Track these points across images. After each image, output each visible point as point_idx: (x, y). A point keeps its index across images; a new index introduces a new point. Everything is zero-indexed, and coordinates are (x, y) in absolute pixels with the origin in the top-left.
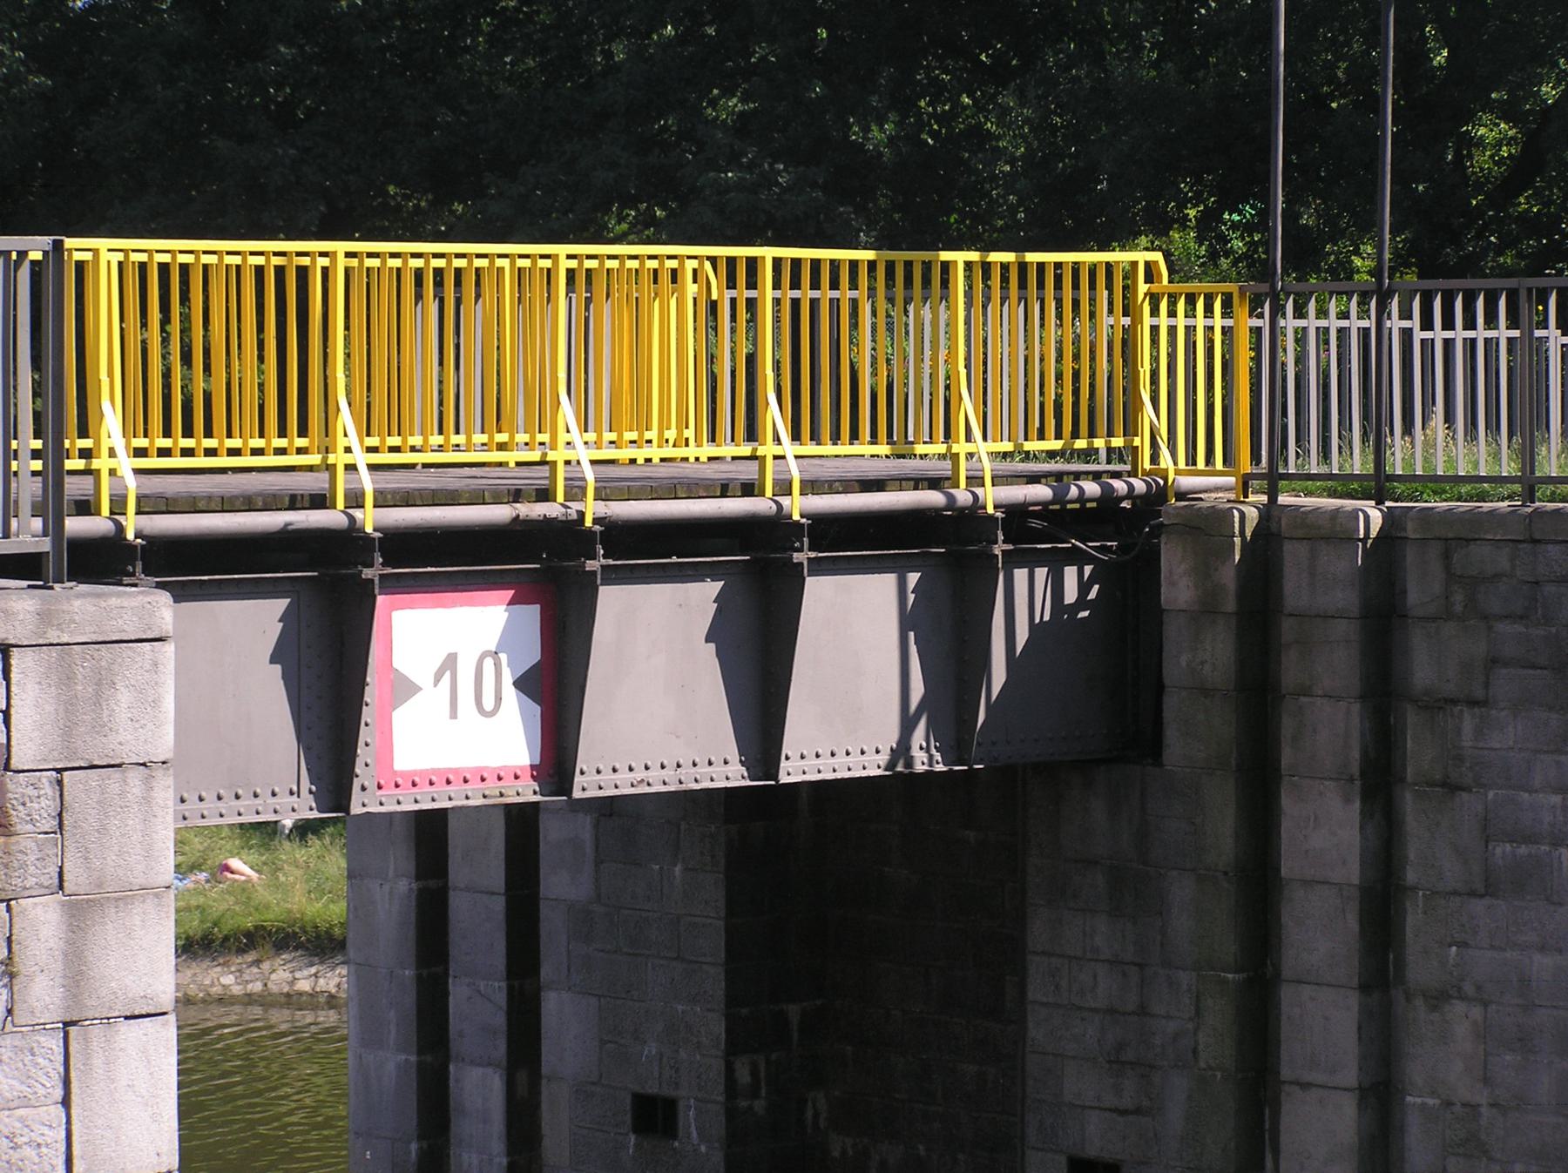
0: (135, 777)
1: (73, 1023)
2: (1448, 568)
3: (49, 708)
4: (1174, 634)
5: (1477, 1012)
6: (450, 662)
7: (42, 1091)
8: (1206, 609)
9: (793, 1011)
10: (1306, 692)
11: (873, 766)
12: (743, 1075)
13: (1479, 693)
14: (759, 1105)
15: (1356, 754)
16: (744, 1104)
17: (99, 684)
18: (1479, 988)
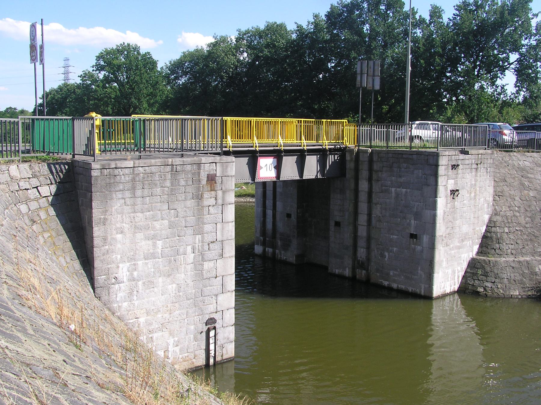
4: (348, 163)
5: (380, 206)
8: (351, 160)
12: (299, 211)
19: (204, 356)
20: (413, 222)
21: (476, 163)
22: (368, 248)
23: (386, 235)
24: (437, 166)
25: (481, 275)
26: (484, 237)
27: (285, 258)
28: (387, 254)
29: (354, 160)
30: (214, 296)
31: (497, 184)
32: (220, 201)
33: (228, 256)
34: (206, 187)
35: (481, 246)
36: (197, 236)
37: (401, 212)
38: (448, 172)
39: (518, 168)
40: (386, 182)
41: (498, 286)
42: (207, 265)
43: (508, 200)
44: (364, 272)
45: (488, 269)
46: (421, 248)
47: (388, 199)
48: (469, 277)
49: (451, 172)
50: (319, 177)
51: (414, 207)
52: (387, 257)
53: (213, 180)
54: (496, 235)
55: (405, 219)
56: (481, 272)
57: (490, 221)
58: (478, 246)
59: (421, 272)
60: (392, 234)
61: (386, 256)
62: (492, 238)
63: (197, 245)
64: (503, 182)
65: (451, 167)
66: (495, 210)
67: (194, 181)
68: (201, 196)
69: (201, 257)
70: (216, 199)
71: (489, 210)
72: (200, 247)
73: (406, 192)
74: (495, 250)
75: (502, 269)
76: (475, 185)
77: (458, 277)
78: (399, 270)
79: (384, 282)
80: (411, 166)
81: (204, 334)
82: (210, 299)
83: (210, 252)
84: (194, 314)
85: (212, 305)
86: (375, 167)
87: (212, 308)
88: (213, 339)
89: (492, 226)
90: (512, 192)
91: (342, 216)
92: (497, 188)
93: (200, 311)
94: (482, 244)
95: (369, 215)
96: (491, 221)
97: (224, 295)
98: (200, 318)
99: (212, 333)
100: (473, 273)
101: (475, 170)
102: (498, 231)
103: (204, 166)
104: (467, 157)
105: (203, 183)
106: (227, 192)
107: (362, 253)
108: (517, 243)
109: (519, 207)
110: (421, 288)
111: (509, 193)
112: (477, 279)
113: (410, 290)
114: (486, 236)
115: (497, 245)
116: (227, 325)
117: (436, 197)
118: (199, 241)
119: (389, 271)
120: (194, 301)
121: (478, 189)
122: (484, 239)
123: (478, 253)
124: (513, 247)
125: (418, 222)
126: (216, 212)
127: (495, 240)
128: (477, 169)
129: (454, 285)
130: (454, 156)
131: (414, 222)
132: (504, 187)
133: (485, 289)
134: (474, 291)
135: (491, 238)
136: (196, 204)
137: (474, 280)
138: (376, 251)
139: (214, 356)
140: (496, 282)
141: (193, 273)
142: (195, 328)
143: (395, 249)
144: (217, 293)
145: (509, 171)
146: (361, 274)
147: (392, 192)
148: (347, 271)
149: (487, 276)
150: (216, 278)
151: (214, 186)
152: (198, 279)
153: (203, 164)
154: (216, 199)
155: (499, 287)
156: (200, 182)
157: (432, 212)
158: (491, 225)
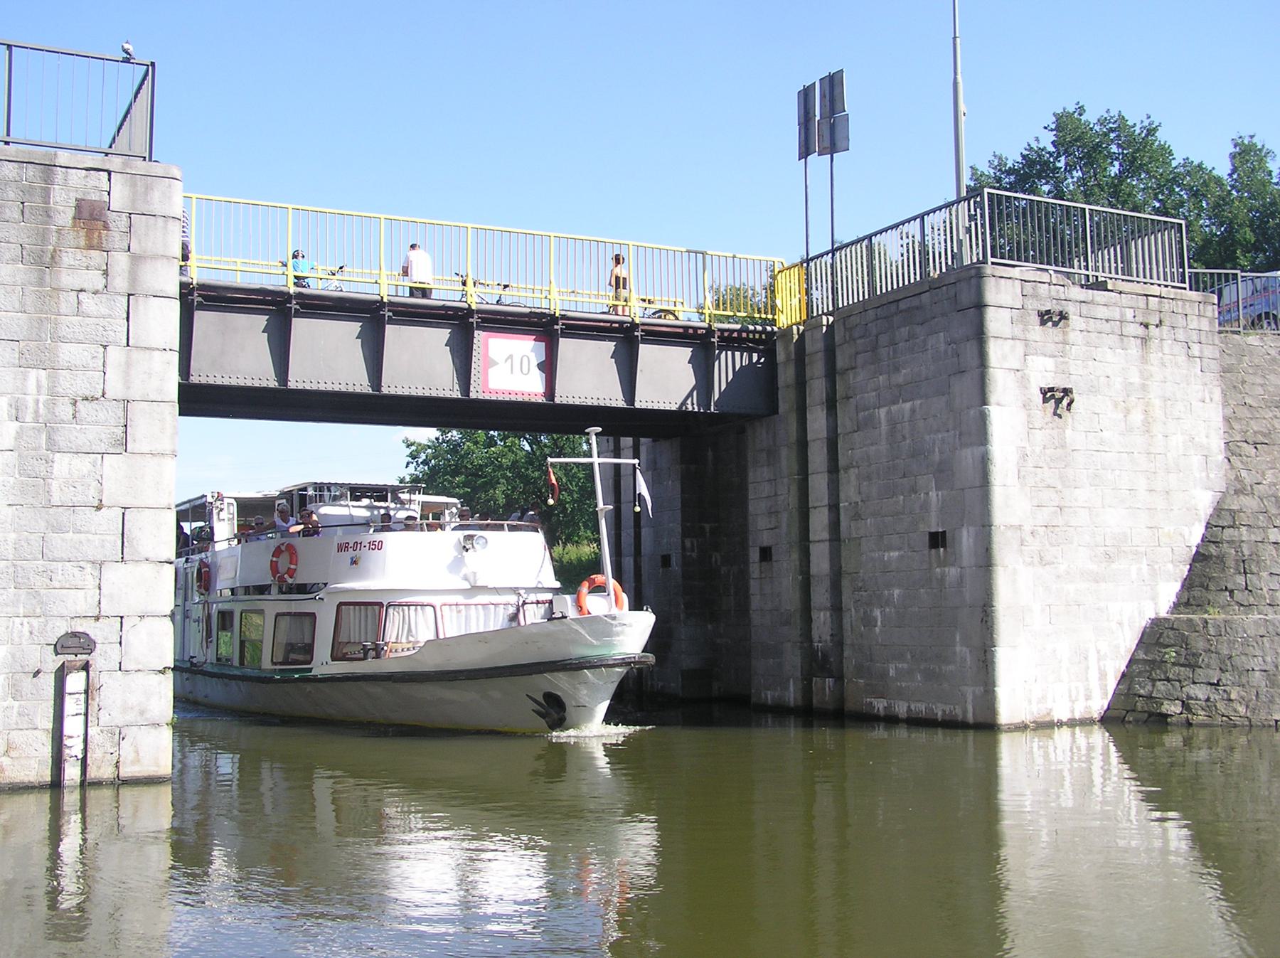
0: (160, 220)
1: (133, 295)
5: (856, 470)
6: (511, 357)
7: (117, 314)
8: (788, 360)
9: (707, 526)
11: (674, 407)
12: (688, 544)
13: (854, 365)
14: (694, 555)
15: (824, 395)
16: (689, 554)
17: (147, 188)
18: (857, 462)
19: (47, 751)
20: (935, 495)
21: (1139, 319)
22: (837, 609)
23: (873, 555)
25: (1174, 664)
27: (661, 684)
28: (877, 613)
30: (89, 565)
31: (1252, 414)
32: (120, 282)
34: (70, 237)
35: (1188, 584)
36: (33, 373)
37: (904, 476)
40: (866, 395)
41: (1229, 694)
42: (62, 464)
44: (829, 682)
45: (1200, 645)
46: (959, 570)
47: (872, 444)
48: (1140, 674)
49: (1037, 332)
50: (690, 409)
51: (934, 451)
52: (879, 623)
53: (97, 220)
54: (1238, 549)
55: (916, 493)
56: (1174, 654)
57: (1218, 510)
59: (964, 649)
60: (890, 548)
61: (876, 622)
62: (1222, 561)
63: (30, 401)
64: (1273, 408)
66: (1237, 478)
67: (26, 211)
68: (53, 257)
69: (44, 436)
70: (106, 273)
71: (1212, 476)
72: (41, 405)
73: (913, 411)
74: (1231, 592)
75: (1245, 643)
76: (1144, 387)
77: (1103, 675)
78: (909, 657)
79: (875, 702)
80: (918, 329)
81: (48, 681)
83: (78, 427)
84: (9, 609)
86: (840, 363)
87: (82, 602)
88: (78, 700)
89: (1226, 524)
91: (775, 528)
92: (1252, 422)
93: (34, 602)
95: (834, 507)
97: (130, 566)
98: (31, 626)
99: (75, 682)
100: (1153, 662)
101: (1139, 341)
102: (1244, 539)
103: (66, 175)
105: (61, 222)
107: (822, 621)
110: (966, 702)
112: (1163, 677)
113: (940, 714)
114: (1204, 555)
115: (1240, 580)
116: (140, 667)
117: (984, 401)
118: (39, 387)
119: (886, 665)
120: (11, 570)
121: (1157, 402)
122: (1197, 565)
123: (1176, 607)
125: (945, 492)
127: (1232, 564)
128: (1145, 340)
129: (1088, 698)
131: (937, 495)
133: (1186, 706)
134: (1151, 714)
135: (1221, 558)
136: (34, 278)
137: (1154, 681)
138: (853, 610)
140: (1224, 681)
141: (12, 480)
142: (13, 656)
143: (896, 592)
144: (100, 558)
146: (825, 687)
147: (880, 423)
148: (792, 689)
149: (1193, 666)
151: (100, 237)
152: (31, 500)
153: (64, 170)
154: (106, 273)
155: (1233, 697)
156: (49, 216)
157: (978, 451)
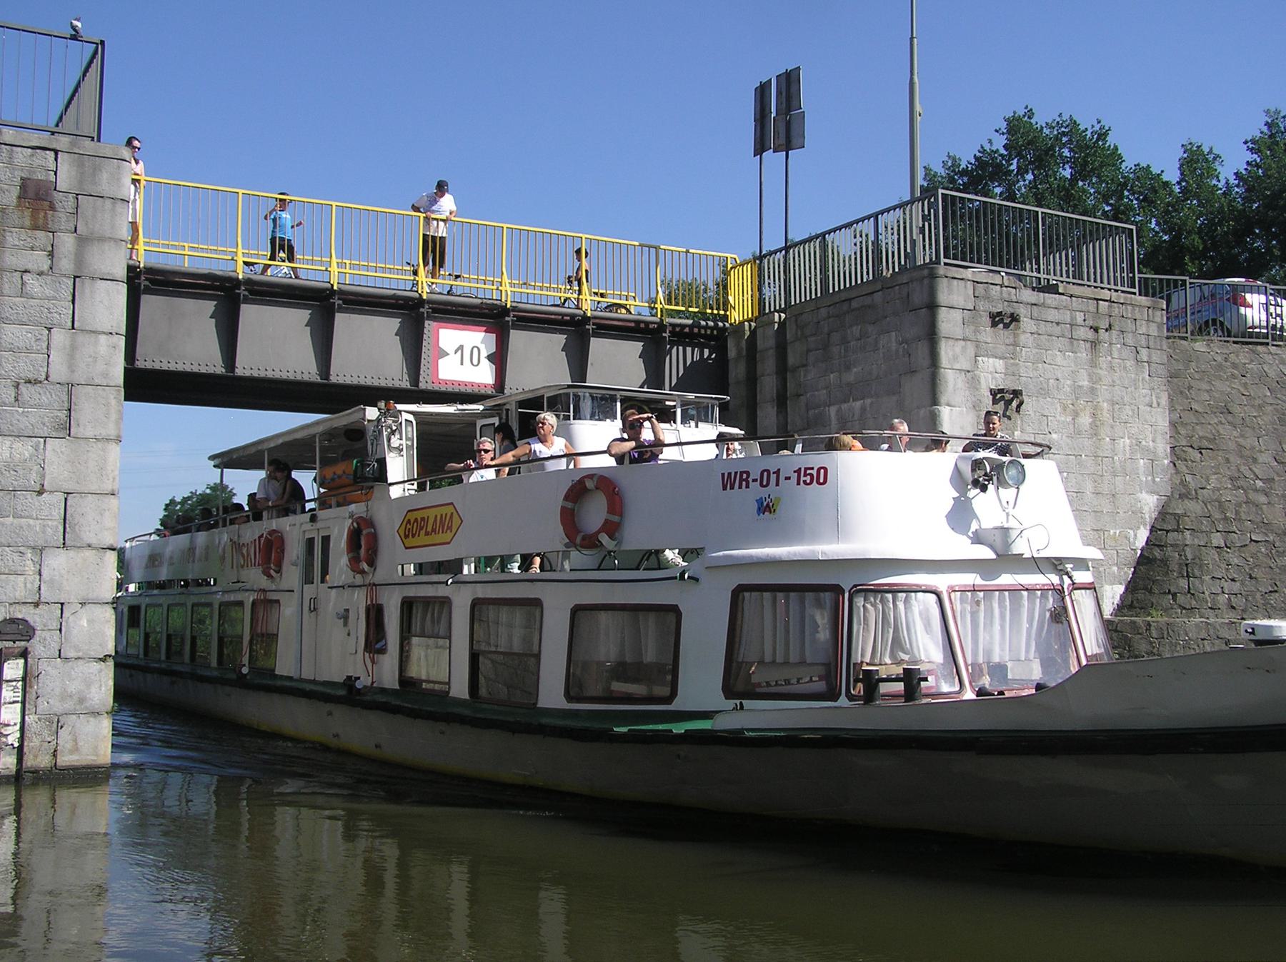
0: (108, 203)
2: (797, 325)
3: (74, 173)
4: (731, 366)
6: (461, 348)
10: (763, 376)
24: (932, 307)
26: (1144, 561)
29: (744, 353)
32: (66, 265)
33: (89, 433)
35: (1131, 587)
38: (976, 331)
39: (1277, 382)
43: (1232, 459)
49: (988, 334)
57: (1163, 514)
58: (1120, 589)
62: (1166, 564)
65: (988, 321)
74: (1174, 595)
76: (1093, 390)
80: (870, 328)
82: (16, 557)
85: (21, 578)
90: (1250, 441)
92: (1198, 427)
94: (1135, 582)
96: (1167, 513)
101: (1088, 345)
102: (1187, 543)
104: (1050, 299)
106: (106, 246)
108: (1251, 577)
109: (1269, 481)
111: (1236, 442)
115: (1183, 583)
116: (80, 654)
117: (935, 401)
124: (1236, 587)
126: (49, 292)
127: (1176, 567)
128: (1094, 344)
130: (998, 287)
132: (1220, 428)
135: (1165, 562)
139: (16, 745)
144: (41, 543)
145: (1247, 389)
150: (40, 493)
154: (51, 255)
158: (1163, 527)
